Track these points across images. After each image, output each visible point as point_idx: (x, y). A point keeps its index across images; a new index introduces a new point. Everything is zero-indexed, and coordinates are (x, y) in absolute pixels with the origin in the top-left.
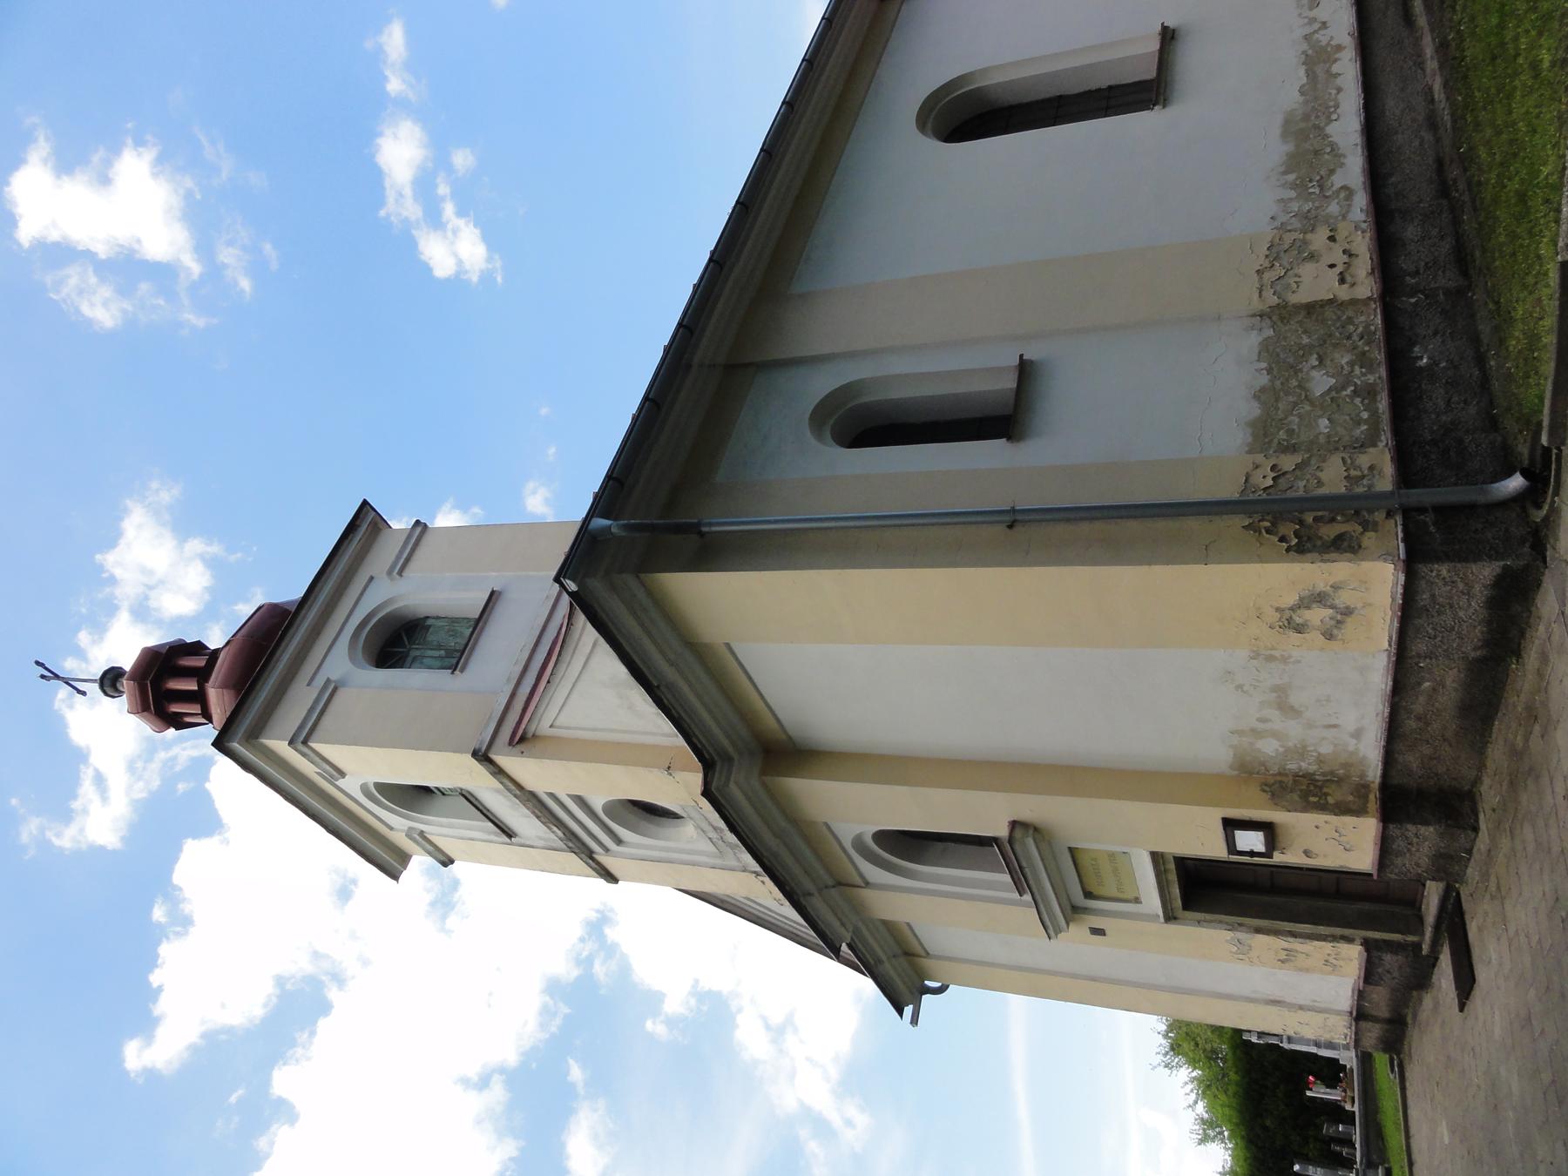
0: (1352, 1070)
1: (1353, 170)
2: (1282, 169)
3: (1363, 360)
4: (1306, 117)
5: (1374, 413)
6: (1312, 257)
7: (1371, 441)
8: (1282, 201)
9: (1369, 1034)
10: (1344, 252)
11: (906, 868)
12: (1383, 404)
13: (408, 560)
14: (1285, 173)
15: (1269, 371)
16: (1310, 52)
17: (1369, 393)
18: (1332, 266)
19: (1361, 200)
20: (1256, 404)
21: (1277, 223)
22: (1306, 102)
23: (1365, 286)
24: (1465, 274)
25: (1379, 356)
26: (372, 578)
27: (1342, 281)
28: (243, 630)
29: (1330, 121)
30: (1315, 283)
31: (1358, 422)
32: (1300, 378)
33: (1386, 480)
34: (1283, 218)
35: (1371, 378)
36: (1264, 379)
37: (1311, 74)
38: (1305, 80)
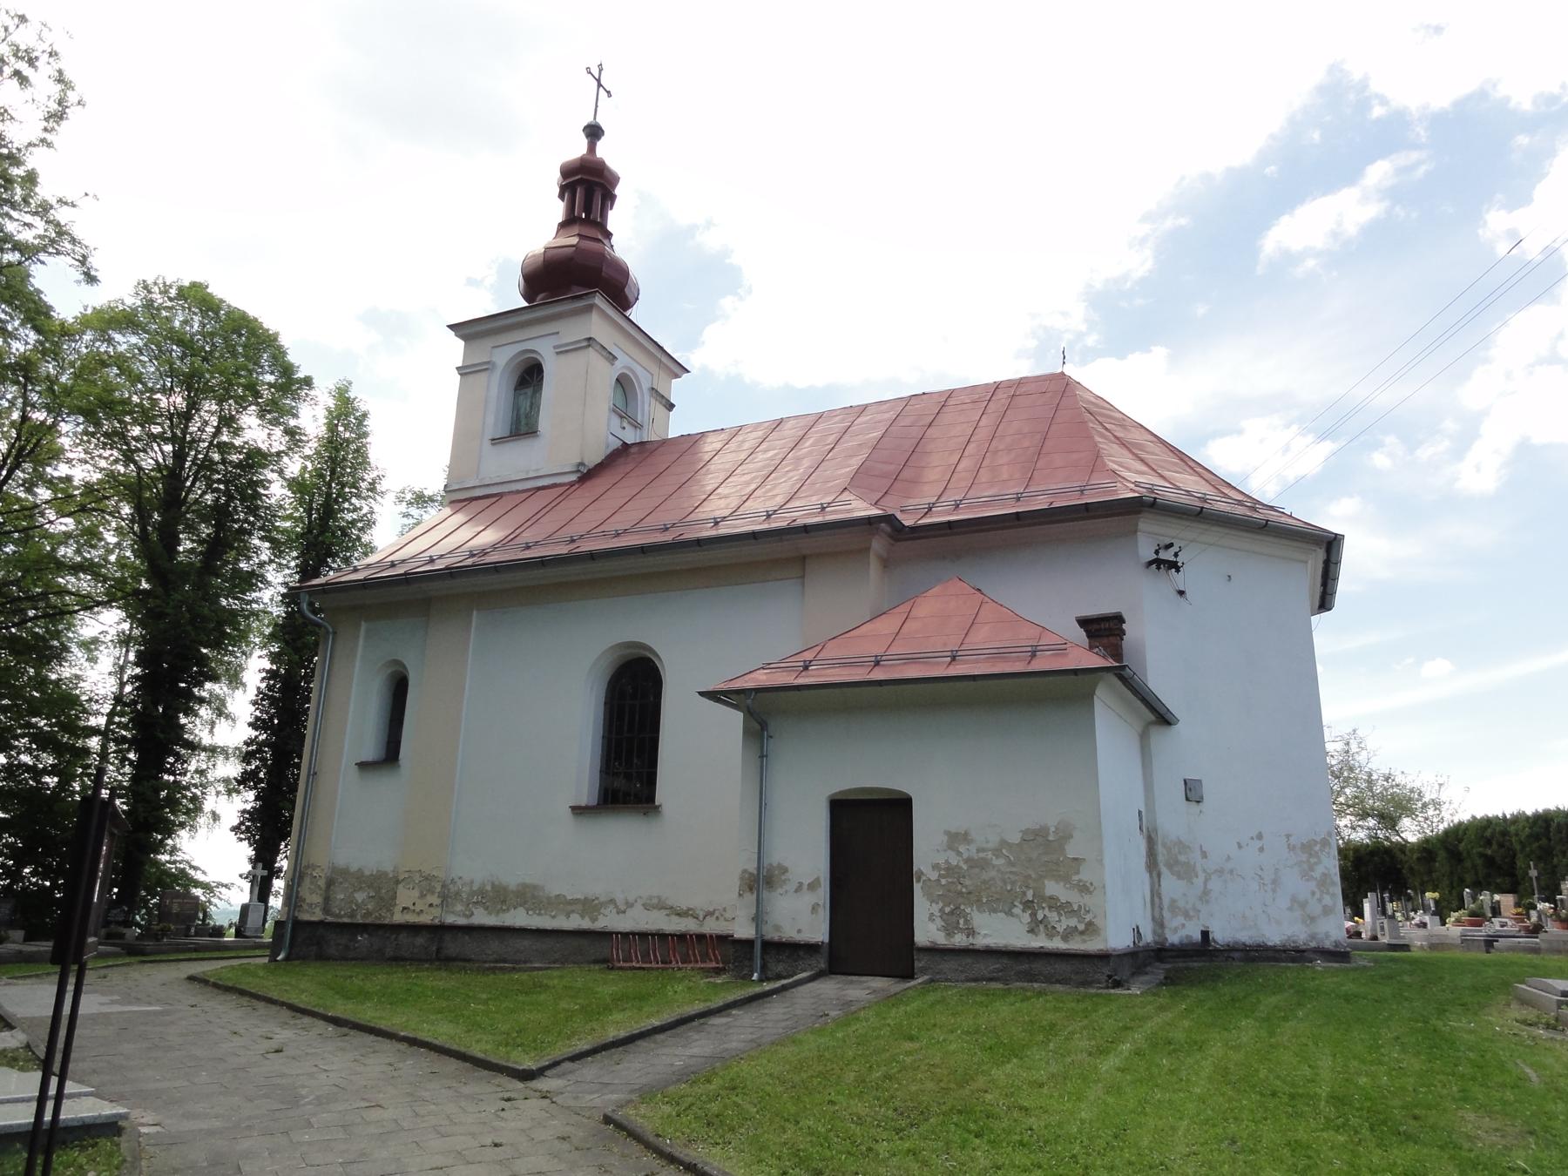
0: (262, 937)
1: (482, 918)
2: (497, 883)
3: (369, 913)
4: (534, 897)
5: (342, 917)
6: (422, 896)
7: (326, 910)
8: (472, 882)
9: (488, 1047)
10: (422, 911)
11: (358, 637)
12: (346, 920)
13: (567, 351)
14: (493, 884)
15: (372, 875)
16: (596, 902)
17: (352, 915)
18: (414, 904)
19: (462, 921)
20: (356, 869)
21: (456, 879)
22: (549, 898)
23: (399, 918)
24: (388, 959)
25: (369, 920)
26: (558, 333)
27: (404, 908)
28: (560, 250)
29: (527, 910)
30: (405, 897)
31: (340, 910)
32: (1040, 916)
33: (305, 917)
34: (459, 883)
35: (359, 917)
36: (367, 873)
37: (575, 901)
38: (569, 898)
